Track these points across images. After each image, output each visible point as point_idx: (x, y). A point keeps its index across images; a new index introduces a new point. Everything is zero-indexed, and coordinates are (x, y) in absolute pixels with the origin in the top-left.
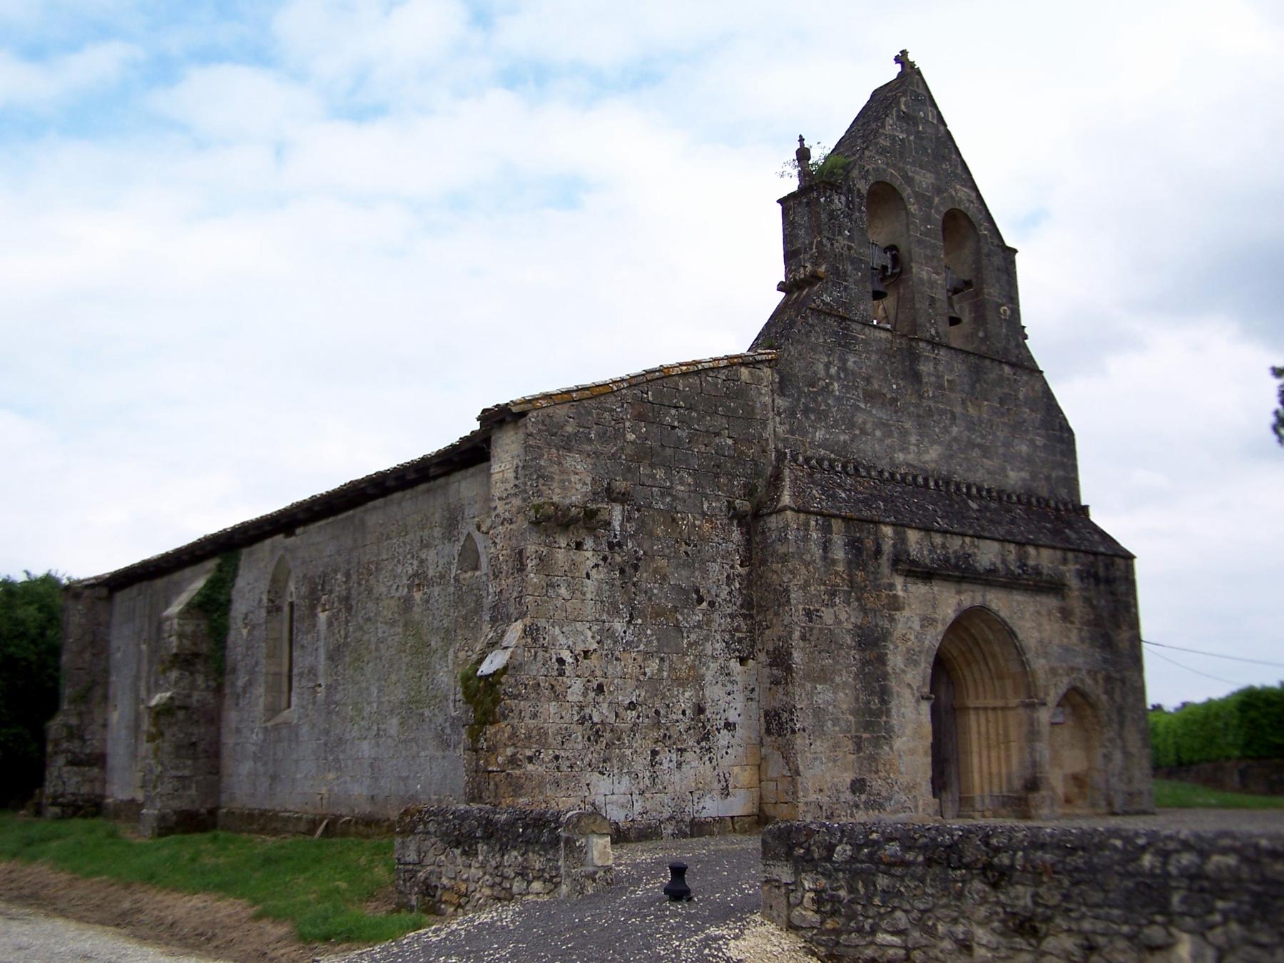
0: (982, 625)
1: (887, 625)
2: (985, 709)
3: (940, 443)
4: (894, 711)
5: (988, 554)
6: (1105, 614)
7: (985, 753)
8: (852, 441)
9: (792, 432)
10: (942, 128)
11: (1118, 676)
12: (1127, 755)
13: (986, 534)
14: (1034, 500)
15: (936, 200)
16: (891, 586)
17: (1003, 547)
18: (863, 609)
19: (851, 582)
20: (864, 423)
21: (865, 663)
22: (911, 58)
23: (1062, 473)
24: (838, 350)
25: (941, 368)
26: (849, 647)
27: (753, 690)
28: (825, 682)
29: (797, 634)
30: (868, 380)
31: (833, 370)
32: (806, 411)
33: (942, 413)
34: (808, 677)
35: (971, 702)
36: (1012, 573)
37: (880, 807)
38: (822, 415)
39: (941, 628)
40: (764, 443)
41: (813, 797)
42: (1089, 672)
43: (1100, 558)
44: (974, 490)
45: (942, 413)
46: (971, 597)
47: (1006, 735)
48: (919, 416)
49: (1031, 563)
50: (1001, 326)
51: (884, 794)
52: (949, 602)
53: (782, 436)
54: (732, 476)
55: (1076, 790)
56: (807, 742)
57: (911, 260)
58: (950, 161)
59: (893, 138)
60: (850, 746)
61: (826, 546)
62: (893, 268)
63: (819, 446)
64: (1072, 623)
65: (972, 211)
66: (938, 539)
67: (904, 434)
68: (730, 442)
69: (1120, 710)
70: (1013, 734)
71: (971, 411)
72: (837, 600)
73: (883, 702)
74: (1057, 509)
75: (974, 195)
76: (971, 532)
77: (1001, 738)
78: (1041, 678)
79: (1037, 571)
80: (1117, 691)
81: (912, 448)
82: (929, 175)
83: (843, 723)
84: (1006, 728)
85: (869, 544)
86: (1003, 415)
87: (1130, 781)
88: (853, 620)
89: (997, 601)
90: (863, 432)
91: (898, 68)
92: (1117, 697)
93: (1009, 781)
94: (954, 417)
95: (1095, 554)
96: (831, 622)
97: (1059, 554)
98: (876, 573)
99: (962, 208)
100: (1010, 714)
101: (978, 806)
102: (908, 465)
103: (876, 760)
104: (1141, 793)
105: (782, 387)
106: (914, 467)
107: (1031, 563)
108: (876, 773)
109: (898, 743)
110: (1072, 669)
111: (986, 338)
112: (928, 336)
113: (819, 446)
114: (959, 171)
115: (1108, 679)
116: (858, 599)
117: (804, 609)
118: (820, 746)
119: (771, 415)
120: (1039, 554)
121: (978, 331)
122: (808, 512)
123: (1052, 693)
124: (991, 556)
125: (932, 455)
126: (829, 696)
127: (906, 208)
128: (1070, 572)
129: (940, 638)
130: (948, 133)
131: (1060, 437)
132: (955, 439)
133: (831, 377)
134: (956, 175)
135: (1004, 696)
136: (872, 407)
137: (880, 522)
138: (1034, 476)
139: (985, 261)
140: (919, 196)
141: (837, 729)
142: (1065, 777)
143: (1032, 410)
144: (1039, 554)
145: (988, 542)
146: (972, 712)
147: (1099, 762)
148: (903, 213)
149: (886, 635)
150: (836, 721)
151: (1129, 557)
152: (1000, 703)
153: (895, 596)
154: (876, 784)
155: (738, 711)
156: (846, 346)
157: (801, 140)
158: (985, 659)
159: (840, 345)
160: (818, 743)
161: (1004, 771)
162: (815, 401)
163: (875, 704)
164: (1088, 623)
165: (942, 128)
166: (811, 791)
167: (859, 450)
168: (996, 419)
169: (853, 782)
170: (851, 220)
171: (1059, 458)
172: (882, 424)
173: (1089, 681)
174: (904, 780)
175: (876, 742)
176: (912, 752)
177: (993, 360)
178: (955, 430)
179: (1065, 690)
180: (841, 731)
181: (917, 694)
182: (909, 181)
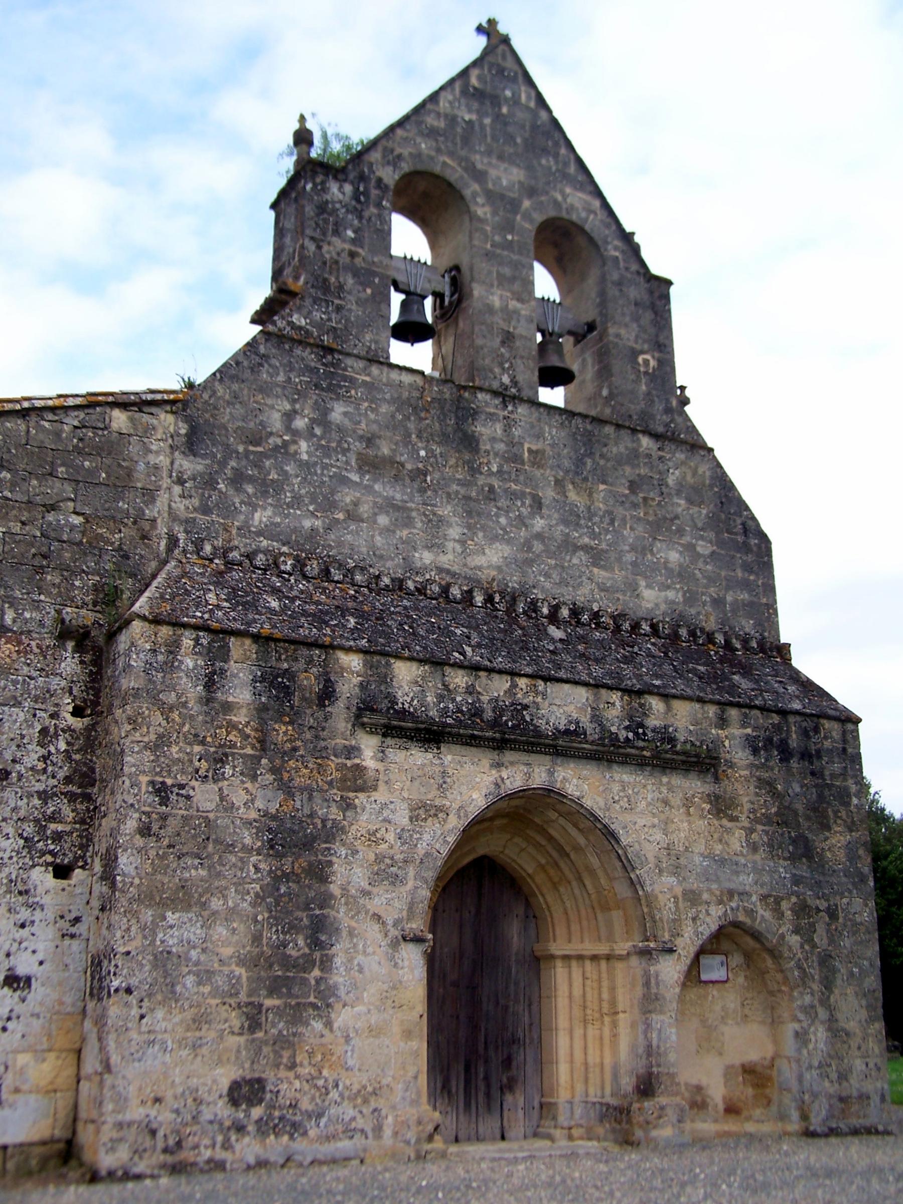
0: (562, 821)
1: (335, 813)
2: (580, 958)
3: (509, 542)
4: (338, 961)
5: (563, 705)
6: (799, 807)
7: (578, 1032)
8: (329, 529)
9: (205, 510)
10: (543, 114)
11: (823, 904)
12: (836, 1032)
13: (562, 674)
14: (683, 632)
15: (527, 204)
16: (351, 751)
17: (597, 698)
18: (287, 789)
19: (262, 741)
20: (356, 504)
21: (278, 878)
22: (502, 28)
23: (744, 596)
24: (313, 395)
25: (517, 432)
26: (249, 850)
27: (77, 920)
28: (188, 908)
29: (131, 825)
30: (370, 440)
31: (300, 423)
32: (238, 480)
33: (514, 496)
34: (148, 897)
35: (558, 947)
36: (614, 738)
37: (296, 1129)
38: (266, 488)
39: (455, 824)
40: (147, 526)
41: (136, 1112)
42: (764, 898)
43: (791, 719)
44: (565, 612)
45: (514, 496)
46: (522, 773)
47: (613, 1002)
48: (467, 498)
49: (653, 722)
50: (637, 381)
51: (305, 1104)
52: (474, 782)
53: (183, 514)
54: (69, 571)
55: (750, 1091)
56: (135, 1012)
57: (472, 279)
58: (556, 156)
59: (452, 120)
60: (236, 1020)
61: (211, 682)
62: (452, 295)
63: (260, 533)
64: (733, 819)
65: (593, 223)
66: (459, 679)
67: (436, 524)
68: (77, 520)
69: (825, 960)
70: (623, 1001)
71: (572, 495)
72: (228, 771)
73: (316, 943)
74: (728, 645)
75: (597, 203)
76: (529, 670)
77: (605, 1005)
78: (666, 908)
79: (666, 736)
80: (821, 929)
81: (450, 545)
82: (515, 171)
83: (219, 980)
84: (613, 989)
85: (309, 680)
86: (635, 506)
87: (843, 1077)
88: (259, 804)
89: (579, 782)
90: (352, 516)
91: (482, 42)
92: (820, 937)
93: (615, 1076)
94: (538, 504)
95: (784, 713)
96: (210, 806)
97: (712, 711)
98: (318, 731)
99: (574, 217)
100: (620, 966)
101: (562, 1119)
102: (440, 570)
103: (291, 1045)
104: (864, 1097)
105: (192, 443)
106: (448, 572)
107: (653, 722)
108: (292, 1066)
109: (342, 1017)
110: (731, 893)
111: (611, 396)
112: (495, 385)
113: (260, 533)
114: (572, 169)
115: (802, 909)
116: (273, 770)
117: (152, 783)
118: (160, 1019)
119: (166, 482)
120: (669, 708)
121: (601, 388)
122: (177, 625)
123: (688, 931)
124: (571, 709)
125: (491, 559)
126: (194, 932)
127: (469, 211)
128: (733, 739)
129: (451, 839)
130: (555, 123)
131: (745, 545)
132: (539, 536)
133: (295, 433)
134: (565, 176)
135: (611, 938)
136: (375, 480)
137: (332, 647)
138: (691, 598)
139: (613, 292)
140: (493, 197)
141: (206, 989)
142: (729, 1071)
143: (690, 502)
144: (669, 708)
145: (566, 687)
146: (559, 963)
147: (789, 1046)
148: (466, 219)
149: (332, 832)
150: (205, 976)
151: (849, 721)
152: (602, 949)
153: (359, 769)
154: (288, 1087)
155: (40, 956)
156: (330, 389)
157: (302, 119)
158: (580, 879)
159: (317, 386)
160: (160, 1014)
161: (608, 1061)
162: (257, 465)
163: (298, 946)
164: (767, 820)
165: (543, 114)
166: (134, 1102)
167: (340, 544)
168: (620, 511)
169: (235, 1086)
170: (360, 218)
171: (739, 573)
172: (390, 506)
173: (764, 913)
174: (354, 1081)
175: (296, 1014)
176: (374, 1031)
177: (618, 426)
178: (539, 524)
179: (714, 927)
180: (214, 993)
181: (394, 932)
182: (480, 176)
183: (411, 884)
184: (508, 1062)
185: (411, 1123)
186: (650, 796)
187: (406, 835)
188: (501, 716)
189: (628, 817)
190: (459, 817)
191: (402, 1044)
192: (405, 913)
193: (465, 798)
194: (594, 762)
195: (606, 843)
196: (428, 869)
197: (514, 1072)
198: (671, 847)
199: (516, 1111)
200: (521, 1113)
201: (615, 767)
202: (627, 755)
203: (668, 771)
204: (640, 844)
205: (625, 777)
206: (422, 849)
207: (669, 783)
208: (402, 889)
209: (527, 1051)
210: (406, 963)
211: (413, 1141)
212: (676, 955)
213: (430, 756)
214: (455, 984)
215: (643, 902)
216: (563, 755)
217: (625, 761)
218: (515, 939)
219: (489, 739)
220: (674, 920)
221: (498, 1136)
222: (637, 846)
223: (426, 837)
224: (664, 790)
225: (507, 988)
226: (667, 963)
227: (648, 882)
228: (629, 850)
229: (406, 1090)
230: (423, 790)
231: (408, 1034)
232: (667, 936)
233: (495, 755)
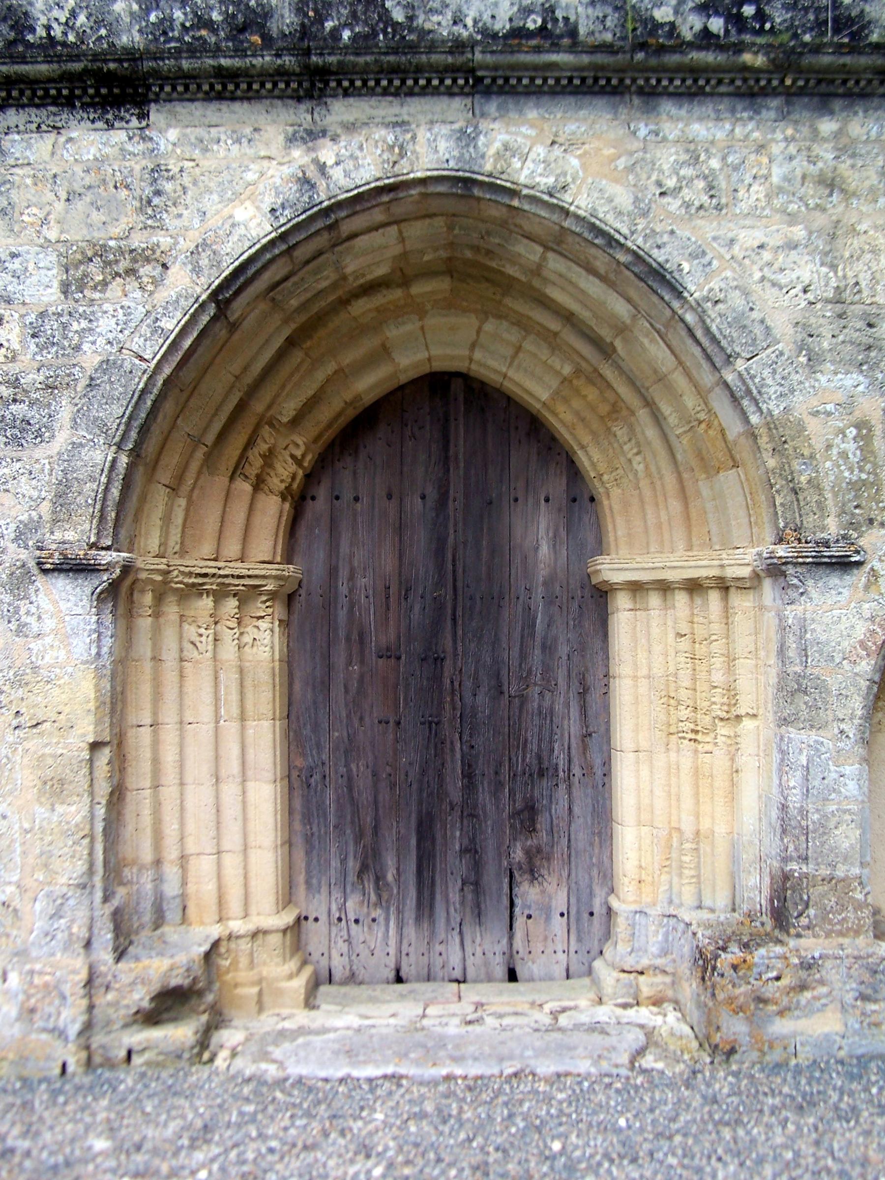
2: (664, 588)
39: (184, 286)
100: (741, 602)
129: (171, 324)
152: (703, 566)
183: (62, 439)
184: (527, 816)
185: (67, 989)
186: (777, 174)
187: (51, 326)
188: (320, 20)
189: (708, 228)
190: (197, 270)
191: (41, 811)
192: (45, 508)
193: (213, 222)
194: (600, 102)
195: (655, 299)
196: (109, 400)
197: (543, 836)
198: (847, 295)
199: (548, 919)
200: (558, 925)
201: (668, 107)
202: (695, 71)
203: (837, 104)
204: (746, 293)
205: (699, 130)
206: (90, 358)
207: (837, 135)
208: (40, 452)
209: (576, 792)
210: (49, 624)
211: (73, 1030)
212: (860, 577)
213: (119, 136)
214: (389, 653)
215: (763, 441)
216: (501, 92)
217: (694, 86)
218: (544, 549)
219: (264, 75)
220: (857, 487)
221: (500, 971)
222: (737, 301)
223: (106, 325)
224: (826, 153)
225: (523, 656)
226: (831, 598)
227: (772, 390)
228: (713, 312)
229: (57, 915)
230: (97, 217)
231: (54, 789)
232: (833, 527)
233: (303, 115)
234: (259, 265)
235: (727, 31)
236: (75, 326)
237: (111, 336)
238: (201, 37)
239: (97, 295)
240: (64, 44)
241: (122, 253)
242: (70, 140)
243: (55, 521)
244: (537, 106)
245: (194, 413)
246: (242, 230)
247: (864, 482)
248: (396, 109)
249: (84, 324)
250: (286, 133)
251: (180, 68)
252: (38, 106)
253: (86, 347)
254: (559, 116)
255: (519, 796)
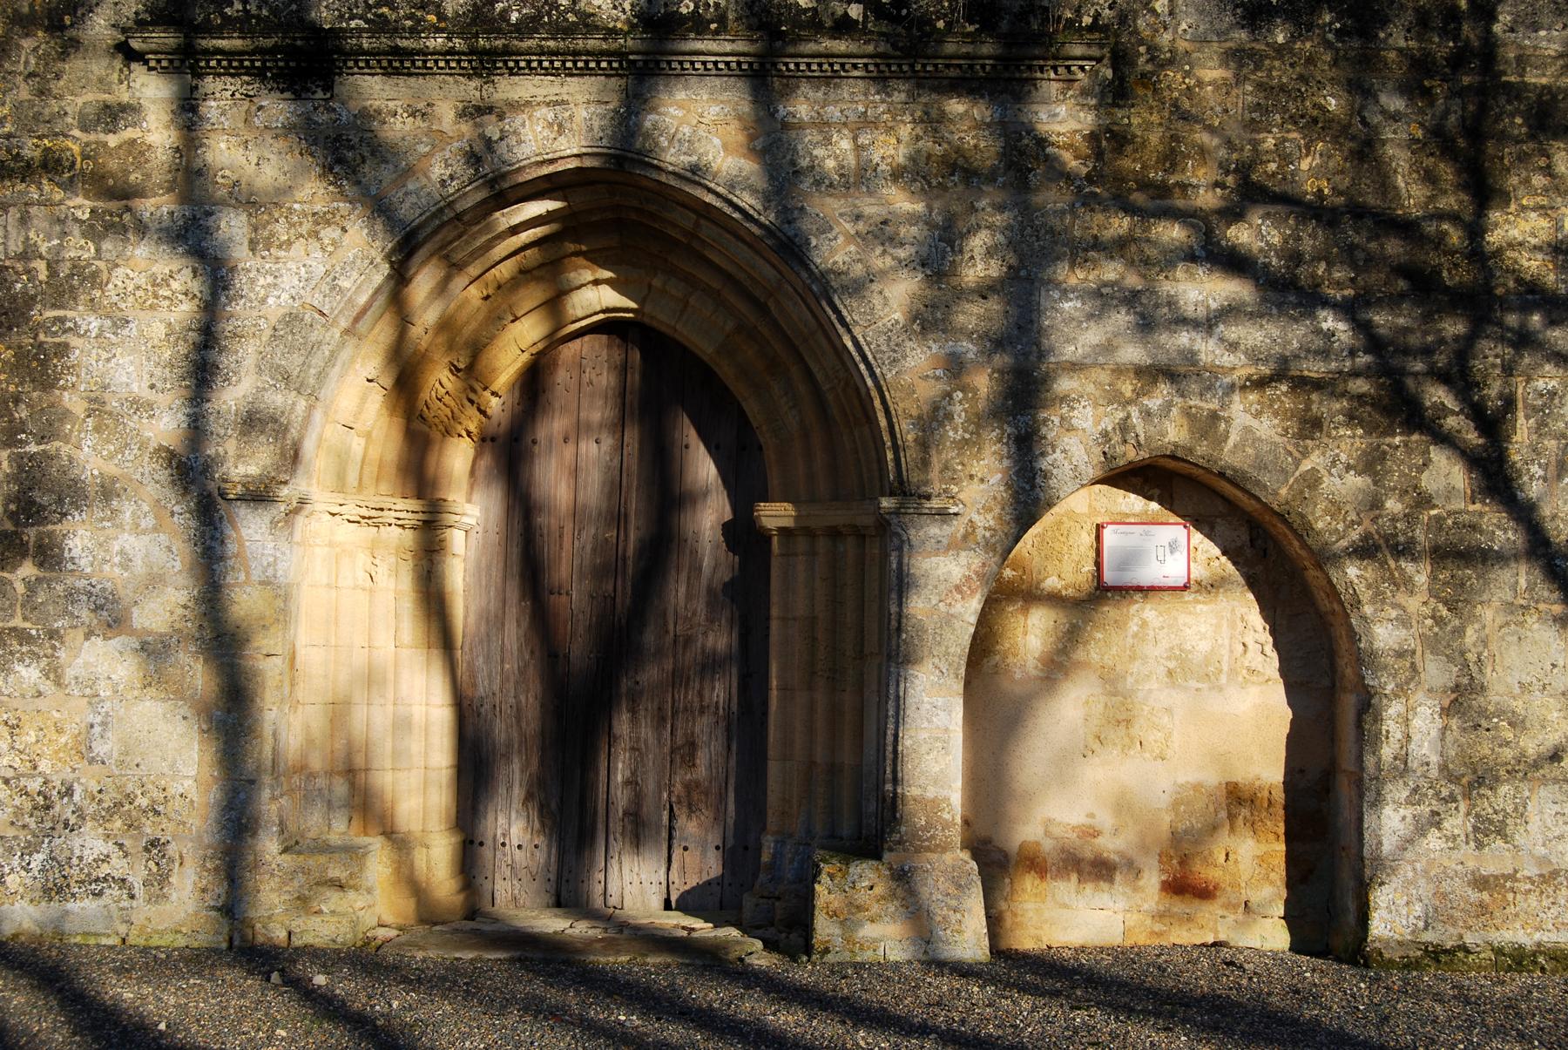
1: (79, 248)
223: (289, 281)
234: (429, 230)
235: (865, 16)
236: (262, 281)
237: (293, 292)
238: (383, 15)
239: (282, 253)
240: (258, 17)
241: (306, 216)
242: (260, 108)
243: (239, 457)
244: (686, 88)
245: (286, 429)
246: (413, 199)
247: (966, 441)
248: (556, 89)
249: (270, 279)
250: (456, 107)
251: (361, 46)
252: (233, 76)
253: (271, 301)
254: (705, 97)
255: (679, 733)
